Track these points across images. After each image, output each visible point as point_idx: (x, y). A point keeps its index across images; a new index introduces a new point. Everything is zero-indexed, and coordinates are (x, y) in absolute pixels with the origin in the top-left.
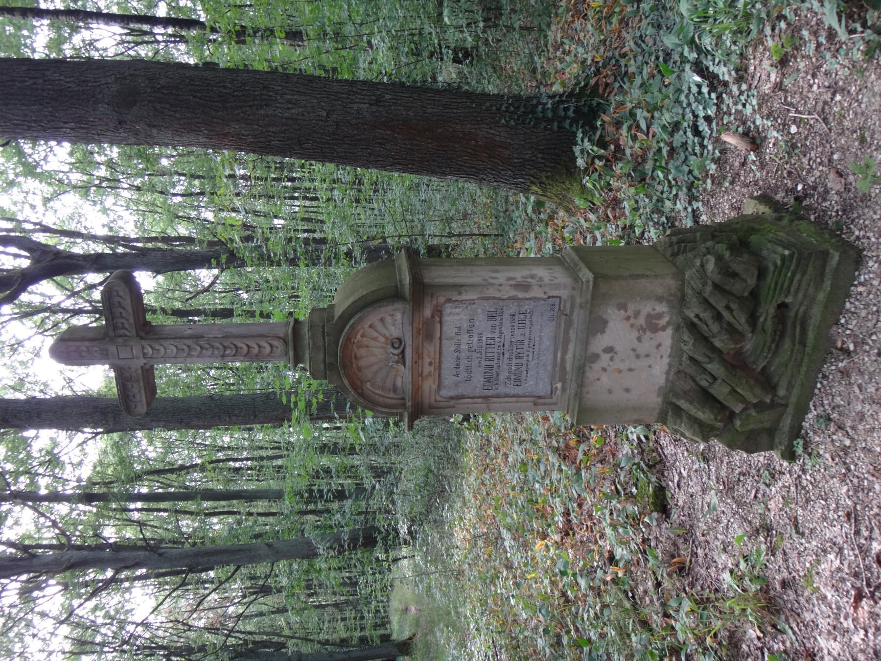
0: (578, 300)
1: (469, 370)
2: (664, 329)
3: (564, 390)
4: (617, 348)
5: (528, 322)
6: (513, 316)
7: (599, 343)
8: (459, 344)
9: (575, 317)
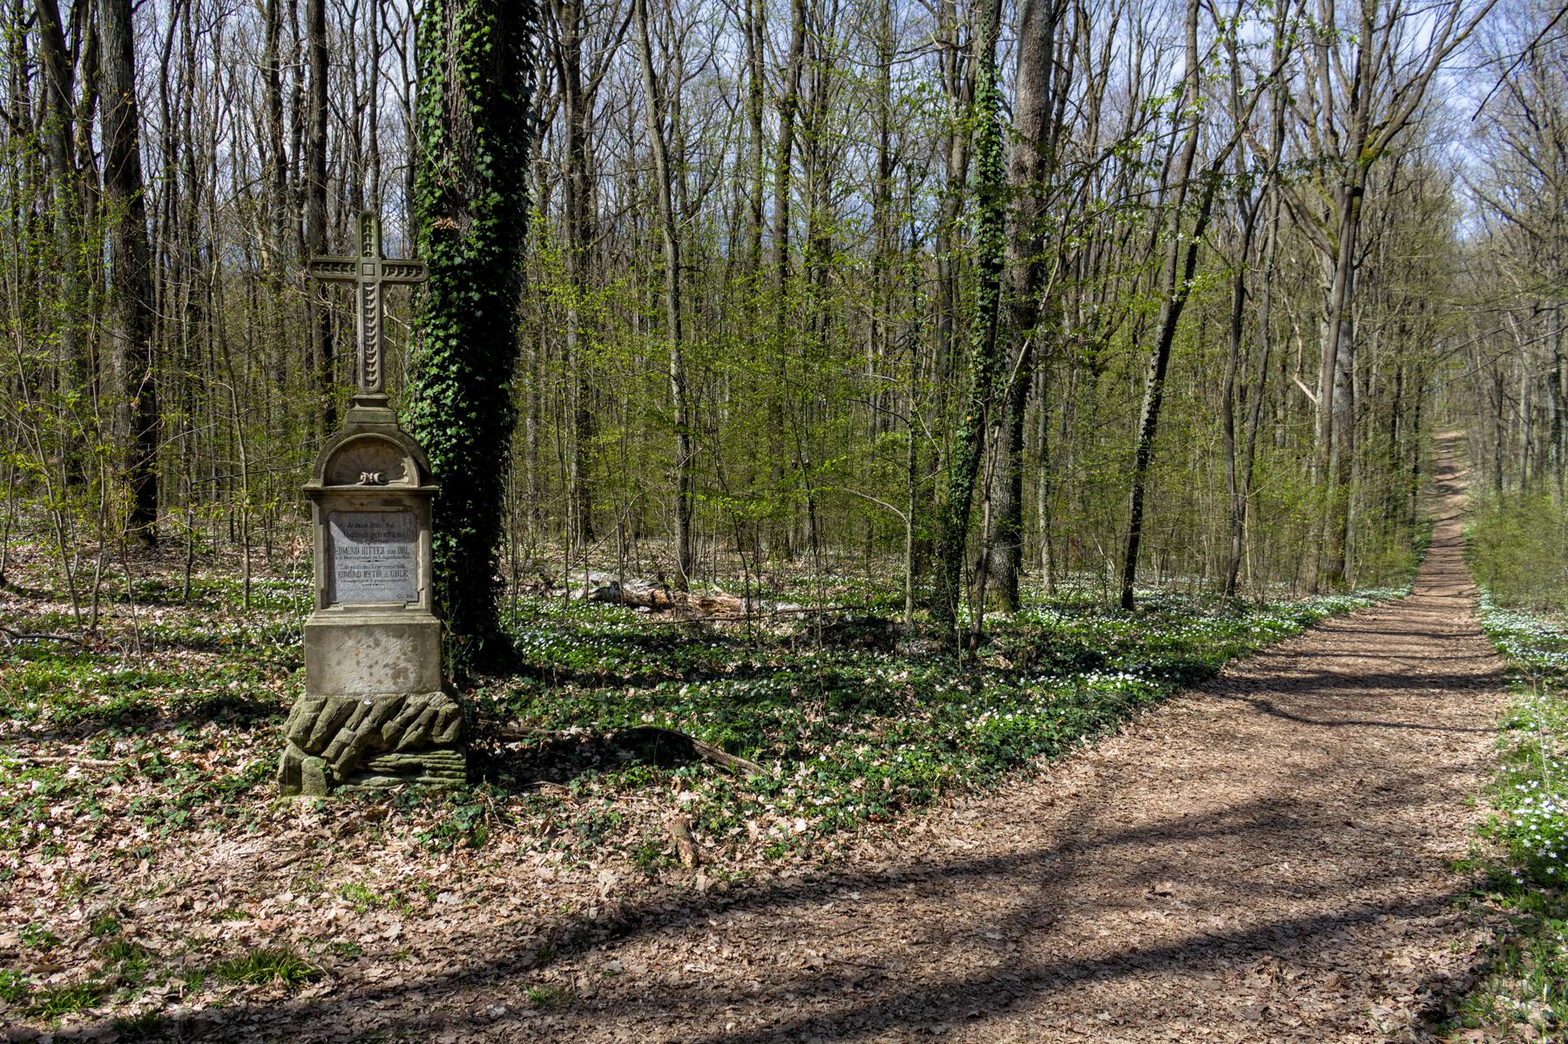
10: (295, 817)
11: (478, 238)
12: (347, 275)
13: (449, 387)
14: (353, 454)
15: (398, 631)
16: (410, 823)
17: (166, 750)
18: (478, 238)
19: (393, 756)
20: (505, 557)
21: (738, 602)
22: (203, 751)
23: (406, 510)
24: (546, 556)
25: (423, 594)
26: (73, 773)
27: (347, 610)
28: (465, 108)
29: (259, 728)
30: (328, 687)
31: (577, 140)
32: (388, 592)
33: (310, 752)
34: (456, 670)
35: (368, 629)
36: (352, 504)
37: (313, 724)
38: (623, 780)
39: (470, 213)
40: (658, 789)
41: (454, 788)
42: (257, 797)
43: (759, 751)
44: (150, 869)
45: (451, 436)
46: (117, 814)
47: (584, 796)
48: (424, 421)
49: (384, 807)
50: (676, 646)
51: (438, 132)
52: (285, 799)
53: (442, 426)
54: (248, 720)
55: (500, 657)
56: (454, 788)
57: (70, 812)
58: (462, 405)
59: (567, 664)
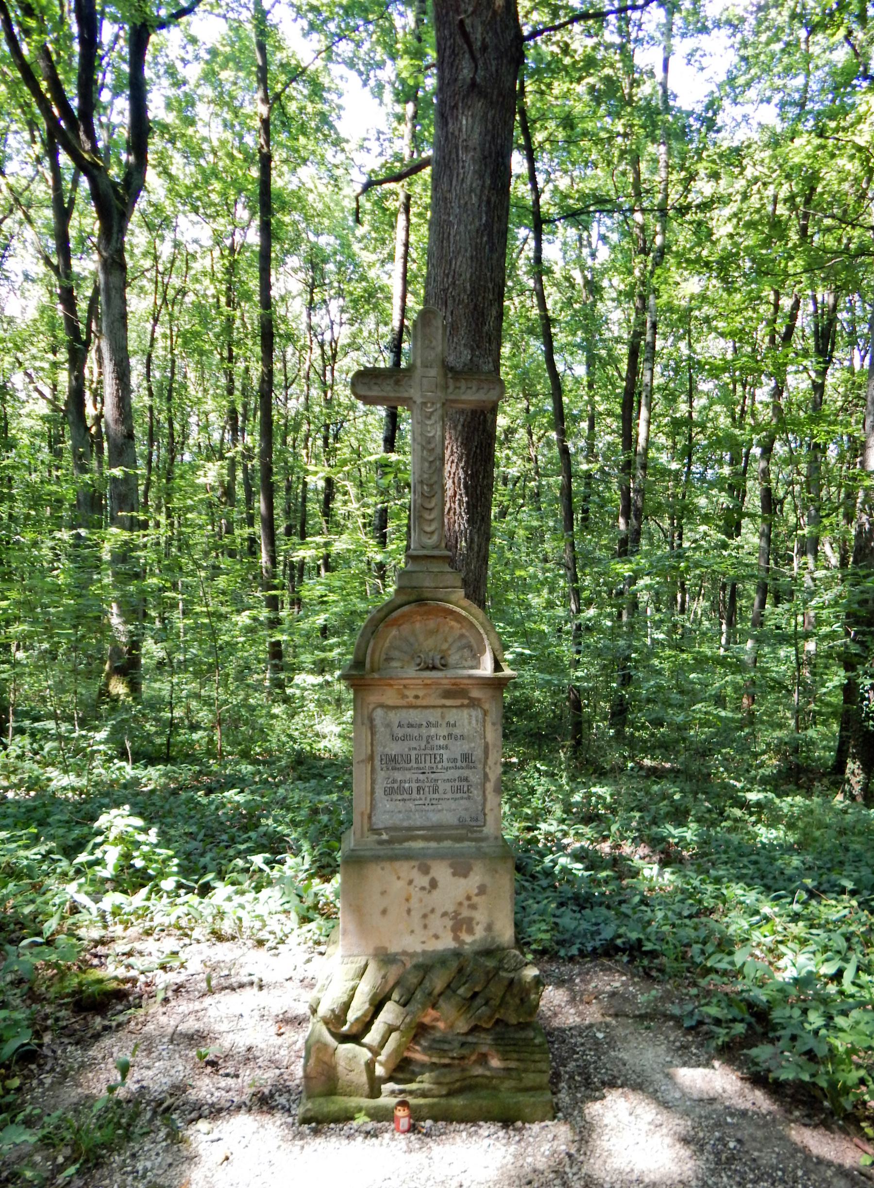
0: (483, 844)
1: (405, 738)
2: (456, 938)
3: (381, 843)
4: (435, 893)
5: (459, 795)
6: (466, 779)
7: (442, 871)
8: (436, 725)
9: (466, 844)
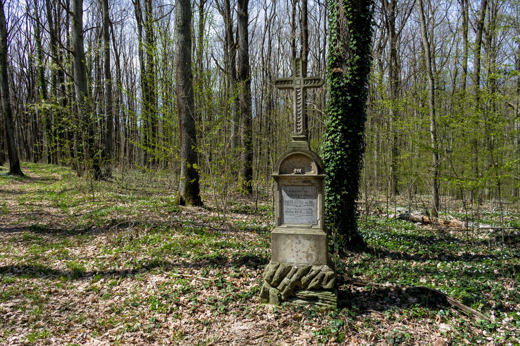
2: (307, 260)
6: (311, 209)
8: (301, 192)
10: (265, 314)
11: (350, 75)
12: (290, 85)
13: (338, 135)
14: (291, 161)
15: (308, 237)
16: (311, 325)
17: (226, 276)
18: (350, 75)
19: (306, 292)
20: (362, 199)
21: (461, 223)
22: (238, 278)
23: (312, 185)
24: (380, 200)
25: (319, 222)
26: (193, 283)
27: (288, 227)
28: (346, 23)
29: (260, 269)
30: (280, 259)
31: (393, 53)
32: (305, 220)
33: (273, 286)
34: (339, 249)
35: (296, 236)
36: (290, 182)
37: (274, 274)
38: (411, 313)
39: (347, 65)
40: (429, 320)
41: (332, 309)
42: (253, 302)
43: (481, 305)
44: (207, 331)
45: (338, 155)
46: (202, 303)
47: (392, 319)
48: (328, 149)
49: (300, 315)
50: (434, 241)
51: (335, 35)
52: (263, 305)
53: (335, 151)
54: (257, 265)
55: (357, 244)
56: (332, 309)
57: (186, 300)
58: (343, 142)
59: (386, 247)
